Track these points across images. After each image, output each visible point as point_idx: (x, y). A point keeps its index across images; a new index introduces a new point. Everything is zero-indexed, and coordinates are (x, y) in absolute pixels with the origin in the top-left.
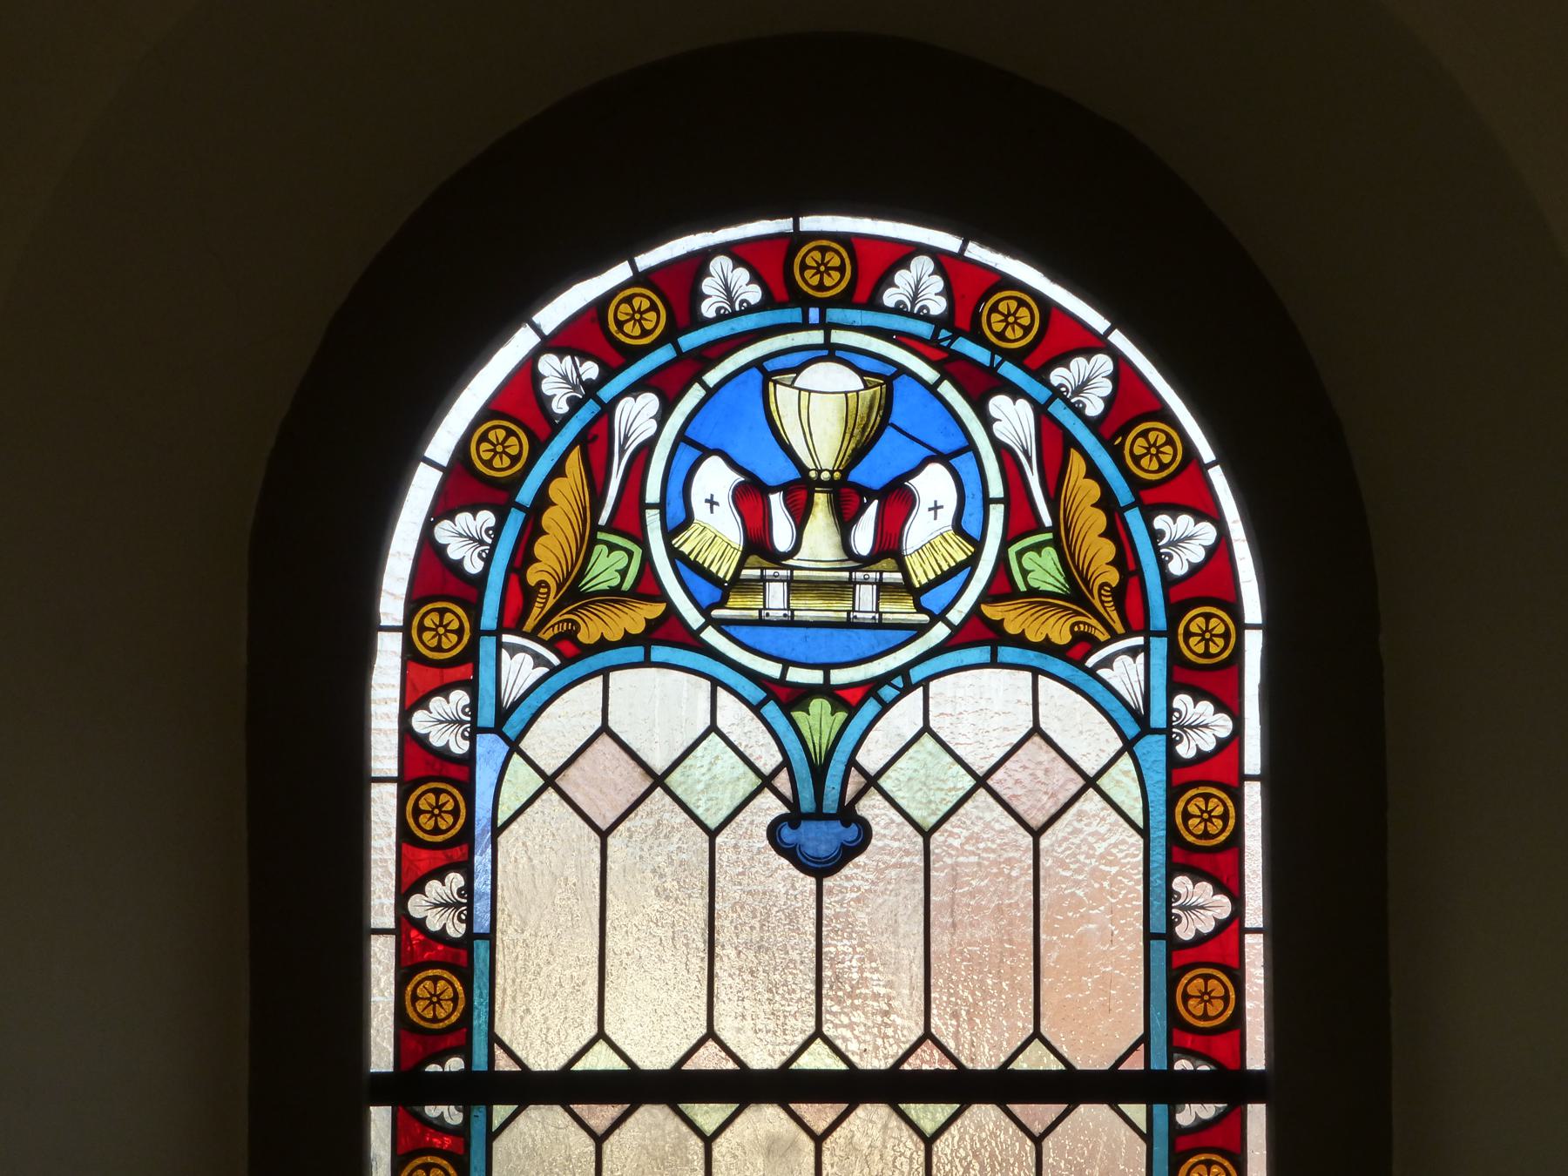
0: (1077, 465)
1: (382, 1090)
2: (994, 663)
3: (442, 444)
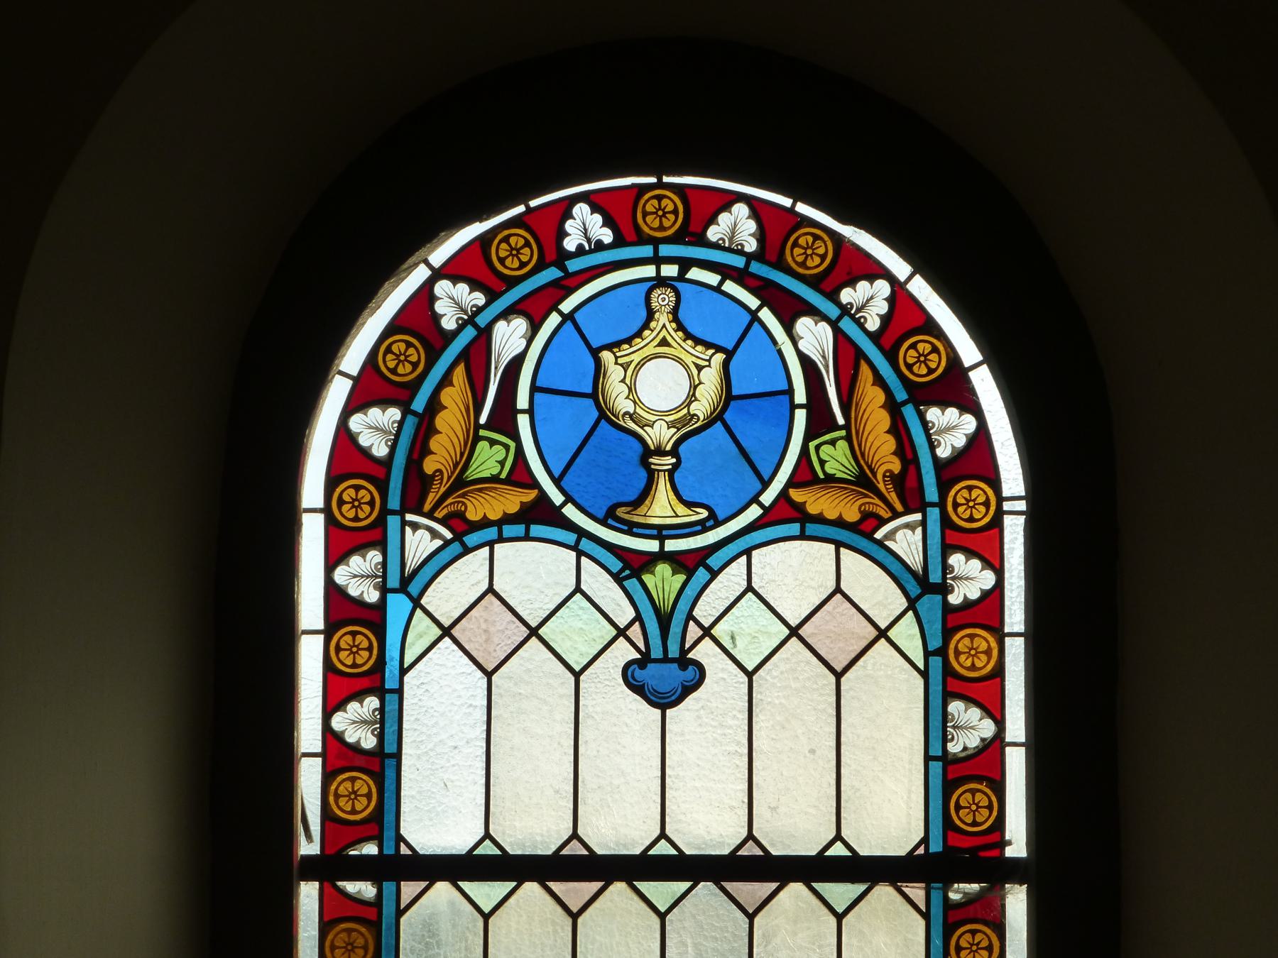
0: (865, 372)
1: (311, 868)
2: (803, 536)
3: (353, 357)
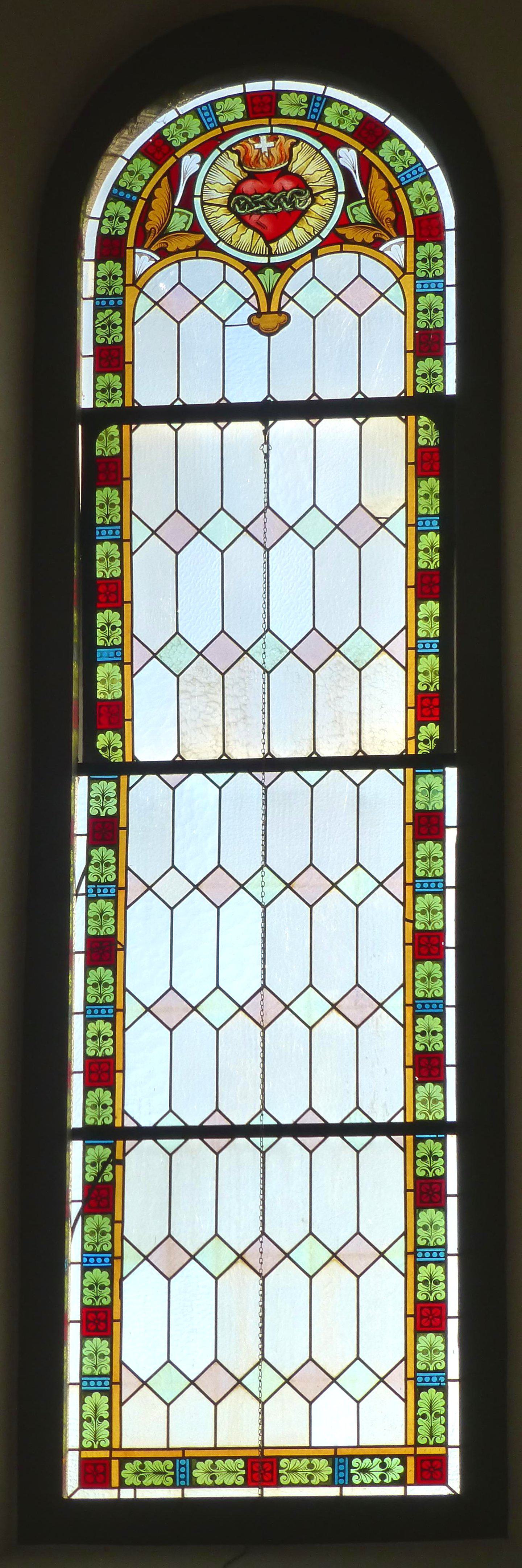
0: (375, 173)
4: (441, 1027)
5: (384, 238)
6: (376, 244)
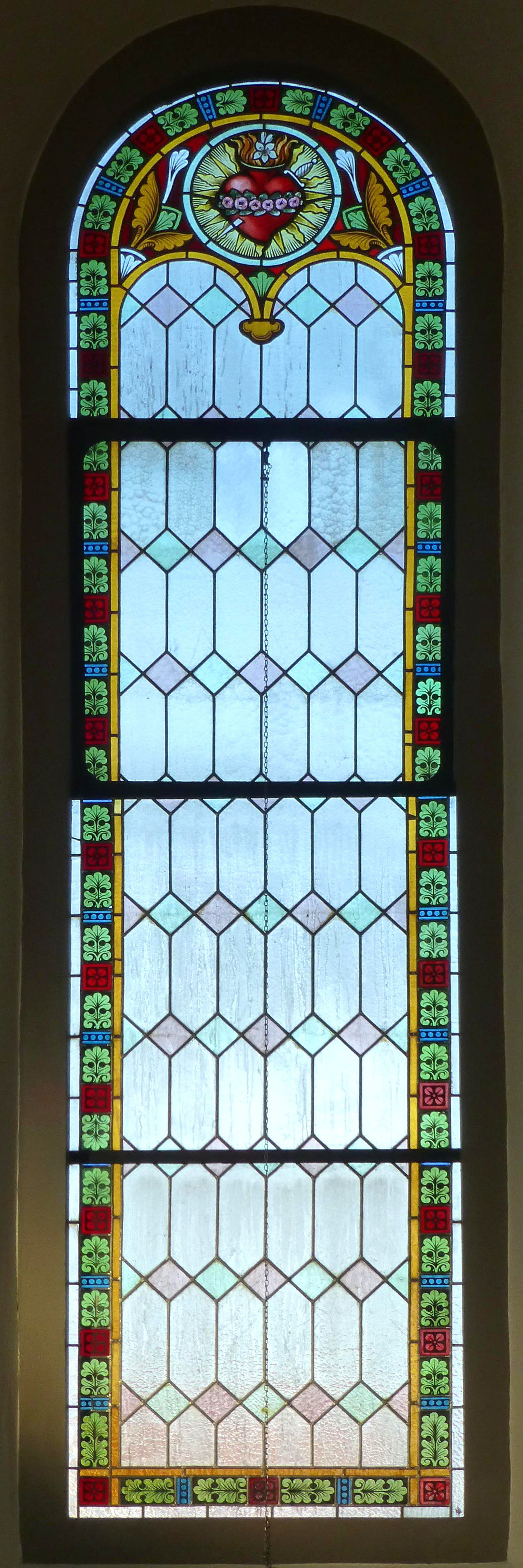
4: (441, 325)
5: (381, 245)
6: (373, 252)
